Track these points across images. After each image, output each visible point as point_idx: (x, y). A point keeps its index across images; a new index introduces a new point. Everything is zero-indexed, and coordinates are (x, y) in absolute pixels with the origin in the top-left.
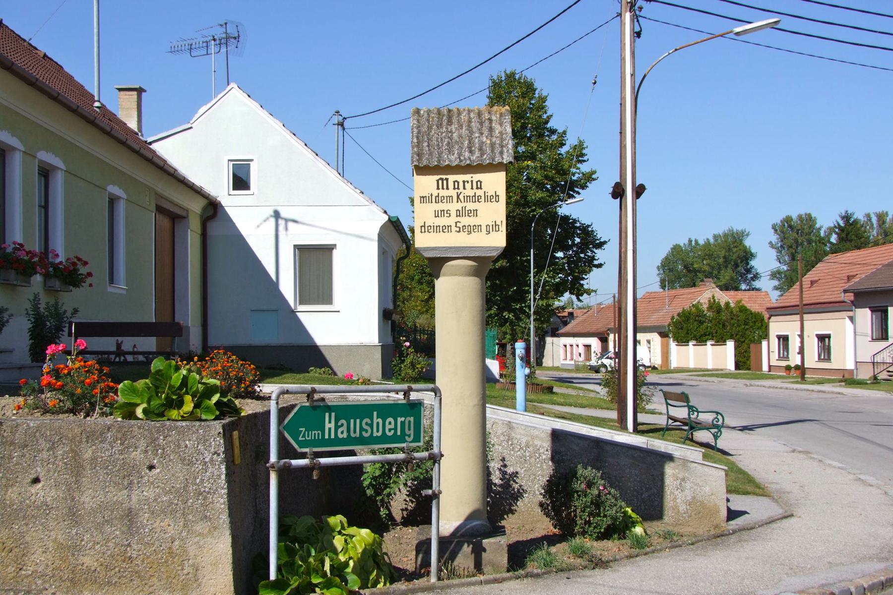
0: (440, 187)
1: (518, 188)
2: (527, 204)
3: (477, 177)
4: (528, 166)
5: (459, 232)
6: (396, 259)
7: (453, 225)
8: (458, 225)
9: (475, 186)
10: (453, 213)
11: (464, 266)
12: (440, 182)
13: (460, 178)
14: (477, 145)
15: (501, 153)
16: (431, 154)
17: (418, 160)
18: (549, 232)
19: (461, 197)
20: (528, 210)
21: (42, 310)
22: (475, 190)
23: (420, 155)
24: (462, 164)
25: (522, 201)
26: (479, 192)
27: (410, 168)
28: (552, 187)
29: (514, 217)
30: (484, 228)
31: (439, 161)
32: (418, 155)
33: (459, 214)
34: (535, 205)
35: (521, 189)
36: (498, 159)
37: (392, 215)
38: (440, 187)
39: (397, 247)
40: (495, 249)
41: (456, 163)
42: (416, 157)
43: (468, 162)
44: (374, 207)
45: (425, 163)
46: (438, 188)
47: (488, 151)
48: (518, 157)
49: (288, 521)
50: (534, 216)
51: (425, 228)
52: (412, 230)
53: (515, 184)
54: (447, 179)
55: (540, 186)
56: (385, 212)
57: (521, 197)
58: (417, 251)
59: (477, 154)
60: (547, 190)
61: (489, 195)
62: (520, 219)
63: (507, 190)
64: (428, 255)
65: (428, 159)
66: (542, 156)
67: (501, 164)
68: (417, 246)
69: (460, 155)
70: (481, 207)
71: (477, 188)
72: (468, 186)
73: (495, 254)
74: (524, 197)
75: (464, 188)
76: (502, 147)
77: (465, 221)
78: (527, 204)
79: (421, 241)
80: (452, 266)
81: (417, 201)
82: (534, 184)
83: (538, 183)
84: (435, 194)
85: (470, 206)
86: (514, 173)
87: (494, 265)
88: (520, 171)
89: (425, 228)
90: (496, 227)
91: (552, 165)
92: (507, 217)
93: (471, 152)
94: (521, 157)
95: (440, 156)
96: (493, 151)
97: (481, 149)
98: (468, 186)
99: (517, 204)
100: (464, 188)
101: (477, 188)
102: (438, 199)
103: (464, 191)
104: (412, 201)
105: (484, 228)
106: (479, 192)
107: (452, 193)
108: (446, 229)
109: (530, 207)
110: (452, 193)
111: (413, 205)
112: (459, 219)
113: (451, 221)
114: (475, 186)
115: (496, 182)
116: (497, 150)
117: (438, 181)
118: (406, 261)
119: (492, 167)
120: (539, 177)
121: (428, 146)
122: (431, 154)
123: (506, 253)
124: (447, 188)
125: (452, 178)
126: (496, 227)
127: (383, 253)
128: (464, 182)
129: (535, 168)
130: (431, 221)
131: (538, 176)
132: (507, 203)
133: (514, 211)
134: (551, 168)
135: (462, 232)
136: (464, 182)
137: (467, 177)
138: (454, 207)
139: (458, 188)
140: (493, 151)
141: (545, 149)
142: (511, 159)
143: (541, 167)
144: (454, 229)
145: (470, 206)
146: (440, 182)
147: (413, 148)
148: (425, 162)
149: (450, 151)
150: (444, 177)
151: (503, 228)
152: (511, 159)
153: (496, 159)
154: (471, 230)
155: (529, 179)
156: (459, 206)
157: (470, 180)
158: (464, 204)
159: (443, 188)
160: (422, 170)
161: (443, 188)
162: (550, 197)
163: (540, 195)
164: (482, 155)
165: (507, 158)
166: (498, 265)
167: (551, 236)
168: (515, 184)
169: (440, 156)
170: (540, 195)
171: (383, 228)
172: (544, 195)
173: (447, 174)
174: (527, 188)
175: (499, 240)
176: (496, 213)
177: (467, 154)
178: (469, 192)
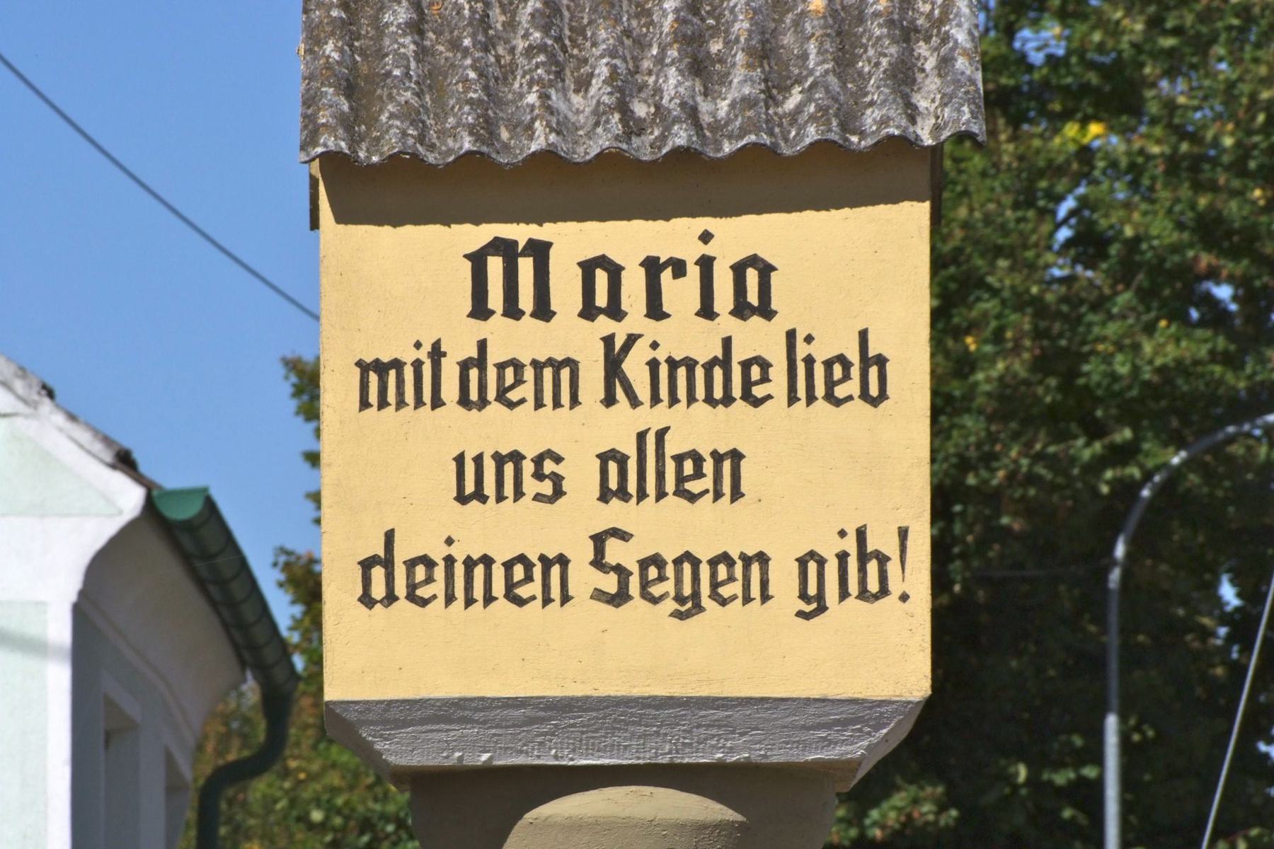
0: (495, 299)
1: (1021, 301)
2: (1080, 411)
3: (738, 235)
4: (1085, 153)
5: (619, 598)
6: (193, 773)
7: (581, 554)
8: (615, 552)
9: (724, 297)
10: (581, 476)
11: (650, 827)
12: (495, 265)
13: (630, 240)
14: (741, 26)
15: (903, 77)
16: (433, 81)
17: (348, 123)
18: (1228, 593)
19: (635, 367)
20: (1085, 450)
21: (284, 632)
22: (726, 323)
23: (358, 87)
24: (644, 148)
25: (1048, 392)
26: (757, 338)
27: (296, 172)
28: (1248, 293)
29: (992, 498)
30: (784, 578)
31: (486, 129)
32: (349, 90)
33: (618, 477)
34: (1130, 413)
35: (1039, 308)
36: (877, 119)
37: (170, 480)
38: (495, 299)
39: (199, 698)
40: (859, 712)
41: (602, 141)
42: (334, 101)
43: (681, 136)
44: (51, 430)
45: (392, 143)
46: (480, 310)
47: (817, 63)
48: (1012, 96)
49: (315, 669)
50: (1127, 490)
51: (392, 575)
52: (306, 583)
53: (1001, 274)
54: (540, 251)
55: (1170, 290)
56: (125, 462)
57: (1041, 365)
58: (339, 725)
59: (742, 81)
60: (1216, 315)
61: (821, 353)
62: (1028, 510)
63: (938, 315)
64: (403, 751)
65: (411, 115)
66: (1178, 90)
67: (899, 147)
68: (332, 693)
69: (625, 88)
70: (766, 433)
71: (741, 310)
72: (681, 294)
73: (857, 748)
74: (1059, 361)
75: (655, 310)
76: (906, 33)
77: (659, 526)
78: (1080, 411)
79: (368, 658)
80: (575, 826)
81: (338, 389)
82: (1124, 274)
83: (1156, 268)
84: (460, 348)
85: (695, 428)
86: (986, 202)
87: (857, 818)
88: (1033, 189)
89: (392, 575)
90: (864, 570)
91: (1243, 151)
92: (944, 499)
93: (701, 68)
94: (1041, 92)
95: (493, 97)
96: (844, 60)
97: (764, 51)
98: (681, 294)
99: (1011, 406)
100: (655, 310)
101: (741, 310)
102: (485, 381)
103: (650, 329)
104: (306, 382)
105: (784, 578)
106: (757, 338)
107: (581, 340)
108: (532, 578)
109: (1095, 431)
110: (581, 340)
111: (311, 412)
112: (617, 514)
113: (565, 528)
114: (724, 297)
115: (863, 272)
116: (877, 56)
117: (478, 260)
118: (260, 787)
119: (838, 175)
120: (1162, 231)
121: (416, 27)
122: (433, 81)
123: (936, 736)
124: (543, 311)
125: (572, 241)
126: (864, 570)
127: (101, 735)
128: (652, 267)
129: (1135, 170)
130: (434, 525)
131: (1153, 224)
132: (945, 408)
133: (989, 459)
134: (1239, 167)
135: (637, 604)
136: (652, 267)
137: (676, 236)
138: (588, 431)
139: (615, 311)
140: (844, 60)
141: (1203, 45)
142: (966, 118)
143: (1173, 164)
144: (584, 578)
145: (695, 428)
146: (495, 265)
147: (314, 38)
148: (391, 136)
149: (562, 66)
150: (520, 233)
151: (916, 577)
152: (966, 118)
153: (870, 118)
154: (693, 584)
155: (1090, 244)
156: (620, 427)
157: (691, 252)
158: (651, 417)
159: (512, 311)
160: (371, 189)
161: (512, 311)
162: (1231, 361)
163: (1165, 347)
164: (774, 88)
165: (940, 110)
166: (884, 817)
167: (1242, 625)
168: (1001, 274)
169: (493, 97)
170: (1165, 347)
171: (104, 568)
172: (1197, 346)
173: (540, 219)
174: (1078, 305)
175: (886, 654)
176: (863, 473)
177: (673, 83)
178: (687, 336)
